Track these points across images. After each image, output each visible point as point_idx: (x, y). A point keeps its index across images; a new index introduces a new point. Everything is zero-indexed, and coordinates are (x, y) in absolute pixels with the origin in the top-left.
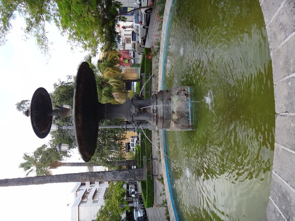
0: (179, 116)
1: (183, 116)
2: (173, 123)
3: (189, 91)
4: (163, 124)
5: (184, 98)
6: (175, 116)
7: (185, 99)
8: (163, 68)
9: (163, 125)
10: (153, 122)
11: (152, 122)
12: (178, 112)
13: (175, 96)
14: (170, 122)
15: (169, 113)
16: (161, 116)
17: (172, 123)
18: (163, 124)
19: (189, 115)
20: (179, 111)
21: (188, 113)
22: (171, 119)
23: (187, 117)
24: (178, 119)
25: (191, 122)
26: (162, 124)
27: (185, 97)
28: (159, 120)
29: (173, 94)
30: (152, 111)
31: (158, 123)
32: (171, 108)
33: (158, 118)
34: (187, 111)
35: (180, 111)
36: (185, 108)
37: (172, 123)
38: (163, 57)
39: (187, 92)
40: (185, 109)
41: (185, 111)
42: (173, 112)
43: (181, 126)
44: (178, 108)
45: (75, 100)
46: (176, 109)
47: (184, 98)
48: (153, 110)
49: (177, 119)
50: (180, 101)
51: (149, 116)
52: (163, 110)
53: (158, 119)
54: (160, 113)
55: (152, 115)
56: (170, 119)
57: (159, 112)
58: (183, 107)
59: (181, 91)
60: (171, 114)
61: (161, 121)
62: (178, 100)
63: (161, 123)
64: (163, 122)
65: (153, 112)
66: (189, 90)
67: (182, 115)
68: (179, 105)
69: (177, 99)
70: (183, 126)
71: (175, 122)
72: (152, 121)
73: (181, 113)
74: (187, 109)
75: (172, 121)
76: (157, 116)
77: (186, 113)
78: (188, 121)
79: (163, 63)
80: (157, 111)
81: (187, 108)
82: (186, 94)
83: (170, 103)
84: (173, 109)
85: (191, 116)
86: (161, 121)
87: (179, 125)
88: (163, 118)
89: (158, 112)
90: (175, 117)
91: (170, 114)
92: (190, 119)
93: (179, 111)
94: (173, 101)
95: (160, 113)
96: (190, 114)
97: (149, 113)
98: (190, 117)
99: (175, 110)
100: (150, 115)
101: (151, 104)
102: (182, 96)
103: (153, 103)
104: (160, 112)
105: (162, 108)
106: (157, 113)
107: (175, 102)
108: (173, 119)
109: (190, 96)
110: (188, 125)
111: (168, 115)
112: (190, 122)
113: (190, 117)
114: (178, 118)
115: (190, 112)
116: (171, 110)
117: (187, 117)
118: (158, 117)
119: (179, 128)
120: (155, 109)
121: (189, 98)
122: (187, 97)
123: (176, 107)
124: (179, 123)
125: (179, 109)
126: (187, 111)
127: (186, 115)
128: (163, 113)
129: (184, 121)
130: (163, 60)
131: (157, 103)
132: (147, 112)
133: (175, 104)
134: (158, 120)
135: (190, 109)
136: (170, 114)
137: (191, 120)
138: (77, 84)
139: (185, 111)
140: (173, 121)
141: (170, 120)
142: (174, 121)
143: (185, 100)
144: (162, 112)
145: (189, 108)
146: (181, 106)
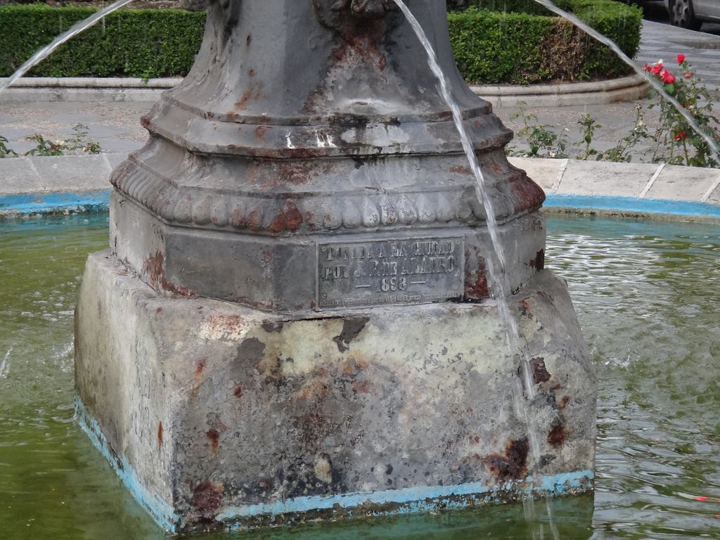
0: (308, 393)
1: (308, 437)
2: (242, 332)
3: (547, 482)
4: (221, 227)
5: (491, 436)
6: (318, 348)
7: (477, 449)
8: (571, 200)
9: (205, 224)
10: (230, 118)
11: (227, 106)
12: (352, 379)
13: (510, 348)
14: (241, 293)
15: (345, 289)
16: (307, 205)
17: (249, 323)
18: (221, 227)
19: (323, 491)
20: (364, 386)
21: (338, 482)
22: (279, 309)
23: (303, 471)
24: (280, 383)
25: (252, 520)
26: (221, 217)
27: (500, 447)
28: (258, 181)
29: (532, 327)
30: (347, 104)
31: (219, 168)
32: (391, 310)
33: (287, 176)
34: (362, 466)
35: (368, 398)
36: (394, 451)
37: (249, 323)
38: (682, 205)
39: (544, 461)
40: (379, 448)
41: (358, 452)
42: (353, 329)
43: (214, 419)
44: (393, 380)
45: (443, 68)
46: (383, 359)
47: (491, 436)
48: (360, 122)
49: (287, 369)
50: (460, 393)
51: (291, 72)
52: (369, 219)
53: (275, 167)
54: (337, 195)
55: (307, 109)
56: (279, 290)
57: (349, 178)
58: (405, 432)
59: (551, 400)
60: (333, 305)
61: (253, 205)
62: (470, 376)
63: (238, 206)
64: (243, 227)
65: (340, 123)
66: (562, 478)
67: (320, 419)
68: (422, 385)
69: (480, 368)
70: (213, 435)
71: (251, 347)
72: (244, 101)
73: (344, 412)
74: (380, 469)
75: (259, 316)
76: (306, 158)
77: (346, 457)
78: (261, 490)
79: (617, 201)
80: (359, 161)
81: (389, 470)
82: (519, 449)
83: (443, 292)
84: (382, 328)
85: (314, 513)
86: (253, 205)
87: (221, 400)
88: (292, 220)
89: (341, 168)
90: (307, 347)
91: (334, 294)
92: (277, 507)
93: (364, 386)
94: (464, 323)
95: (337, 195)
96: (324, 502)
97: (324, 72)
98: (304, 503)
99: (369, 346)
100: (301, 80)
101: (415, 92)
102: (503, 417)
103: (430, 119)
104: (346, 187)
105: (392, 209)
106: (338, 159)
107: (457, 346)
108: (286, 333)
109: (503, 494)
110: (218, 485)
111: (326, 279)
112: (247, 501)
113: (304, 503)
114: (298, 382)
115: (348, 501)
116: (377, 311)
117: (303, 471)
118: (293, 167)
119: (193, 394)
120: (381, 138)
121: (483, 484)
122: (493, 461)
123: (398, 356)
124: (238, 393)
125: (387, 392)
126: (362, 466)
127: (322, 465)
128: (344, 228)
129: (263, 443)
130: (645, 203)
131: (433, 162)
132: (337, 57)
133: (435, 347)
134: (258, 172)
135: (381, 497)
136: (334, 294)
137: (266, 517)
138: (457, 104)
139: (358, 452)
140: (267, 327)
141: (267, 297)
142: (262, 336)
143: (467, 450)
144: (350, 215)
145: (391, 484)
146: (409, 405)
